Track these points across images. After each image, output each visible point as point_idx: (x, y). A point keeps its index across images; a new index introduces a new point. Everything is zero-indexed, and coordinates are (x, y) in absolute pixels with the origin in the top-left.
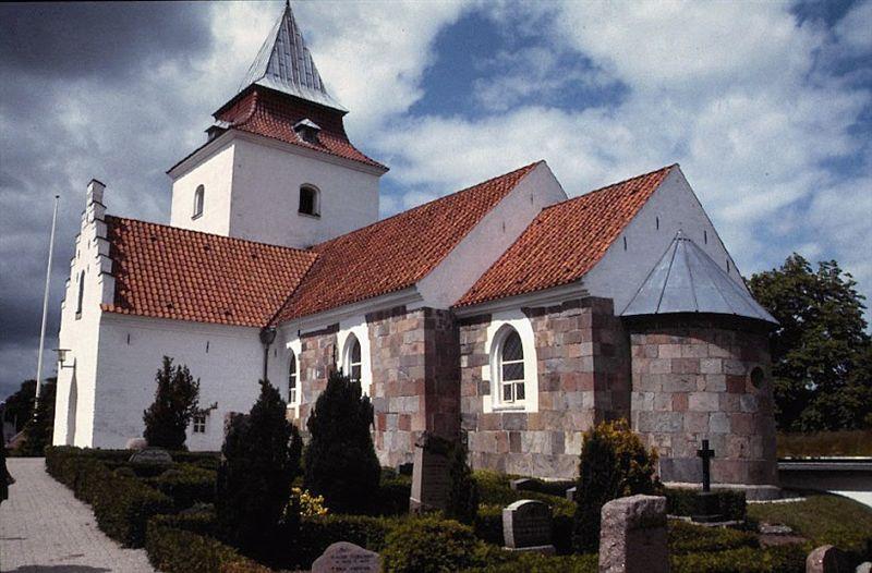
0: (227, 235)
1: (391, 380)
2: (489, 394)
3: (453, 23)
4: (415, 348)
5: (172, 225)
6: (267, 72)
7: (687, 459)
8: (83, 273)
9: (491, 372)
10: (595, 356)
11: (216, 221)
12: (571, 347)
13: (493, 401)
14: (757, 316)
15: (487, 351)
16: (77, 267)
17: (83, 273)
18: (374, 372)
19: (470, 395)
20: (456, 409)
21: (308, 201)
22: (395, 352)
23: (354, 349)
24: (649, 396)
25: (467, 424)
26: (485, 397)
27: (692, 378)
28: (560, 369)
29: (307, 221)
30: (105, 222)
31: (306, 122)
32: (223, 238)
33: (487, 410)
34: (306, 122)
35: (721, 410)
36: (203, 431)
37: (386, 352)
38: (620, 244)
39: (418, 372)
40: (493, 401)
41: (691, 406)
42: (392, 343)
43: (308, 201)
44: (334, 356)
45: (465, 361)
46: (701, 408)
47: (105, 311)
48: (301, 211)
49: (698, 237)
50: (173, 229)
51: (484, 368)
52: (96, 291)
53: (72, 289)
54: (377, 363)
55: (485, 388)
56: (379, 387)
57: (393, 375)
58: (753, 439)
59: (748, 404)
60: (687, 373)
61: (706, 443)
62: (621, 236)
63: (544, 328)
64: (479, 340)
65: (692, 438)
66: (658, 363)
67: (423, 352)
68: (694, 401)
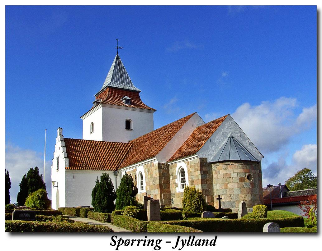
0: (102, 141)
1: (151, 185)
2: (177, 187)
3: (48, 197)
4: (156, 175)
5: (84, 139)
6: (112, 81)
7: (228, 202)
8: (58, 158)
9: (178, 180)
10: (201, 175)
11: (97, 136)
12: (196, 172)
13: (179, 189)
14: (248, 160)
15: (176, 175)
16: (56, 155)
17: (58, 158)
18: (146, 183)
19: (173, 188)
20: (169, 192)
21: (128, 125)
22: (151, 176)
23: (141, 177)
24: (218, 185)
25: (172, 196)
26: (177, 188)
27: (229, 179)
28: (194, 179)
29: (128, 132)
30: (64, 141)
31: (126, 97)
32: (100, 142)
33: (177, 191)
34: (126, 97)
35: (237, 187)
36: (214, 245)
37: (149, 177)
38: (209, 141)
39: (158, 182)
40: (179, 189)
41: (229, 187)
42: (151, 173)
43: (128, 125)
44: (136, 178)
45: (171, 178)
46: (232, 187)
47: (67, 169)
48: (126, 128)
49: (237, 137)
50: (84, 140)
51: (176, 179)
52: (63, 163)
53: (55, 162)
54: (147, 180)
55: (176, 186)
56: (148, 187)
57: (151, 183)
58: (248, 195)
59: (247, 185)
60: (228, 177)
61: (219, 196)
62: (209, 139)
63: (189, 167)
64: (175, 171)
65: (229, 196)
66: (220, 175)
67: (158, 176)
68: (230, 185)
